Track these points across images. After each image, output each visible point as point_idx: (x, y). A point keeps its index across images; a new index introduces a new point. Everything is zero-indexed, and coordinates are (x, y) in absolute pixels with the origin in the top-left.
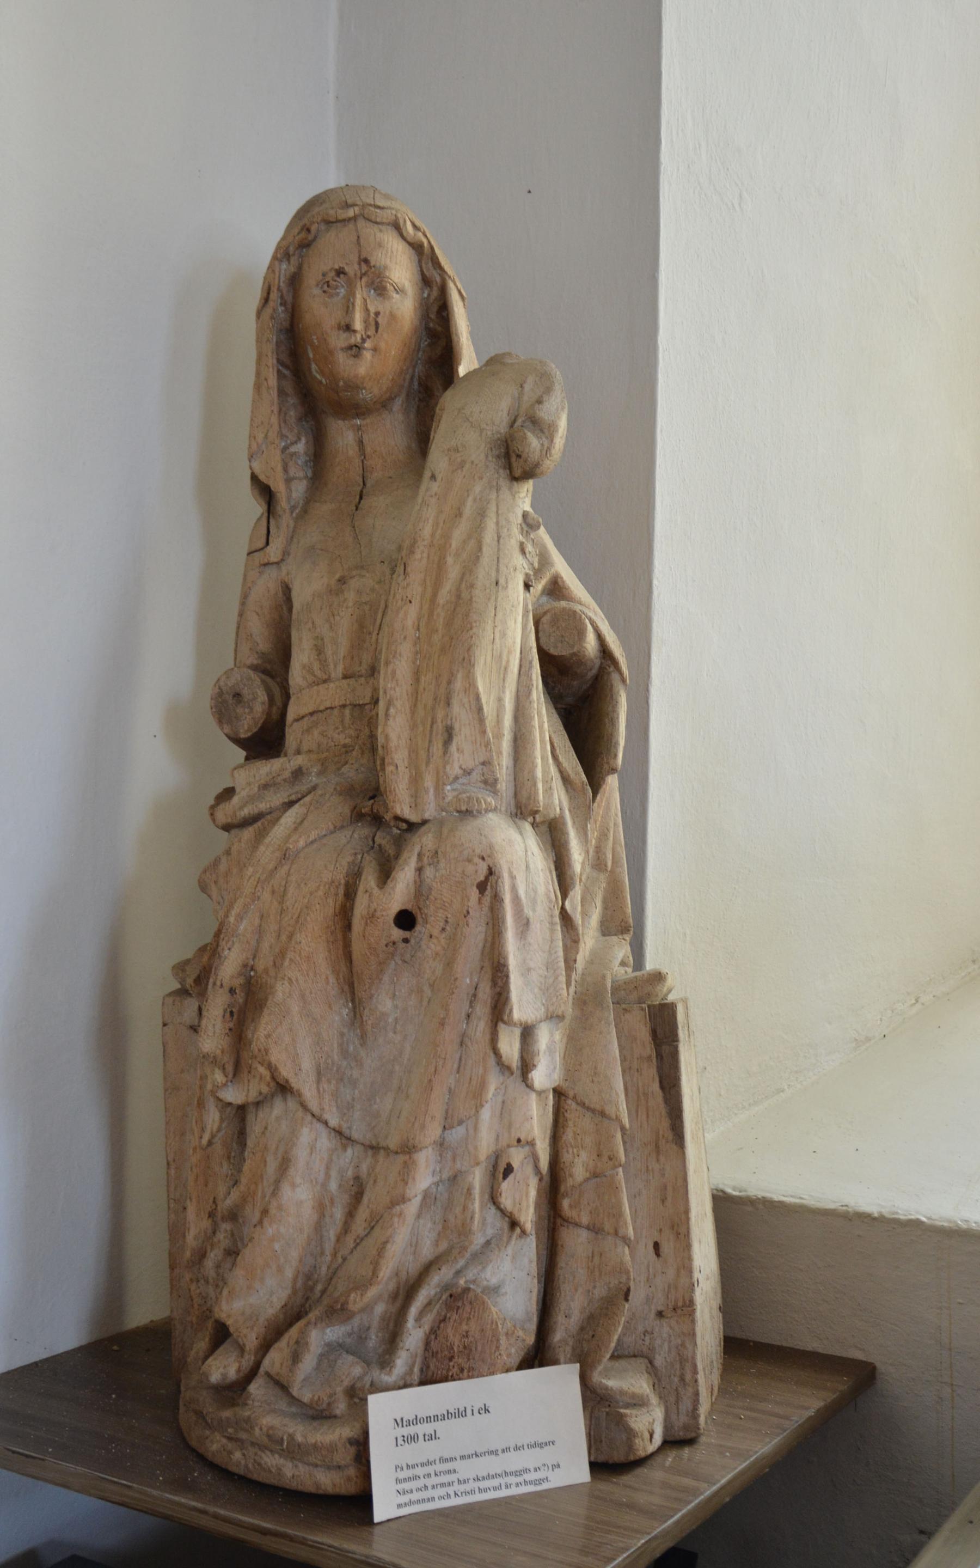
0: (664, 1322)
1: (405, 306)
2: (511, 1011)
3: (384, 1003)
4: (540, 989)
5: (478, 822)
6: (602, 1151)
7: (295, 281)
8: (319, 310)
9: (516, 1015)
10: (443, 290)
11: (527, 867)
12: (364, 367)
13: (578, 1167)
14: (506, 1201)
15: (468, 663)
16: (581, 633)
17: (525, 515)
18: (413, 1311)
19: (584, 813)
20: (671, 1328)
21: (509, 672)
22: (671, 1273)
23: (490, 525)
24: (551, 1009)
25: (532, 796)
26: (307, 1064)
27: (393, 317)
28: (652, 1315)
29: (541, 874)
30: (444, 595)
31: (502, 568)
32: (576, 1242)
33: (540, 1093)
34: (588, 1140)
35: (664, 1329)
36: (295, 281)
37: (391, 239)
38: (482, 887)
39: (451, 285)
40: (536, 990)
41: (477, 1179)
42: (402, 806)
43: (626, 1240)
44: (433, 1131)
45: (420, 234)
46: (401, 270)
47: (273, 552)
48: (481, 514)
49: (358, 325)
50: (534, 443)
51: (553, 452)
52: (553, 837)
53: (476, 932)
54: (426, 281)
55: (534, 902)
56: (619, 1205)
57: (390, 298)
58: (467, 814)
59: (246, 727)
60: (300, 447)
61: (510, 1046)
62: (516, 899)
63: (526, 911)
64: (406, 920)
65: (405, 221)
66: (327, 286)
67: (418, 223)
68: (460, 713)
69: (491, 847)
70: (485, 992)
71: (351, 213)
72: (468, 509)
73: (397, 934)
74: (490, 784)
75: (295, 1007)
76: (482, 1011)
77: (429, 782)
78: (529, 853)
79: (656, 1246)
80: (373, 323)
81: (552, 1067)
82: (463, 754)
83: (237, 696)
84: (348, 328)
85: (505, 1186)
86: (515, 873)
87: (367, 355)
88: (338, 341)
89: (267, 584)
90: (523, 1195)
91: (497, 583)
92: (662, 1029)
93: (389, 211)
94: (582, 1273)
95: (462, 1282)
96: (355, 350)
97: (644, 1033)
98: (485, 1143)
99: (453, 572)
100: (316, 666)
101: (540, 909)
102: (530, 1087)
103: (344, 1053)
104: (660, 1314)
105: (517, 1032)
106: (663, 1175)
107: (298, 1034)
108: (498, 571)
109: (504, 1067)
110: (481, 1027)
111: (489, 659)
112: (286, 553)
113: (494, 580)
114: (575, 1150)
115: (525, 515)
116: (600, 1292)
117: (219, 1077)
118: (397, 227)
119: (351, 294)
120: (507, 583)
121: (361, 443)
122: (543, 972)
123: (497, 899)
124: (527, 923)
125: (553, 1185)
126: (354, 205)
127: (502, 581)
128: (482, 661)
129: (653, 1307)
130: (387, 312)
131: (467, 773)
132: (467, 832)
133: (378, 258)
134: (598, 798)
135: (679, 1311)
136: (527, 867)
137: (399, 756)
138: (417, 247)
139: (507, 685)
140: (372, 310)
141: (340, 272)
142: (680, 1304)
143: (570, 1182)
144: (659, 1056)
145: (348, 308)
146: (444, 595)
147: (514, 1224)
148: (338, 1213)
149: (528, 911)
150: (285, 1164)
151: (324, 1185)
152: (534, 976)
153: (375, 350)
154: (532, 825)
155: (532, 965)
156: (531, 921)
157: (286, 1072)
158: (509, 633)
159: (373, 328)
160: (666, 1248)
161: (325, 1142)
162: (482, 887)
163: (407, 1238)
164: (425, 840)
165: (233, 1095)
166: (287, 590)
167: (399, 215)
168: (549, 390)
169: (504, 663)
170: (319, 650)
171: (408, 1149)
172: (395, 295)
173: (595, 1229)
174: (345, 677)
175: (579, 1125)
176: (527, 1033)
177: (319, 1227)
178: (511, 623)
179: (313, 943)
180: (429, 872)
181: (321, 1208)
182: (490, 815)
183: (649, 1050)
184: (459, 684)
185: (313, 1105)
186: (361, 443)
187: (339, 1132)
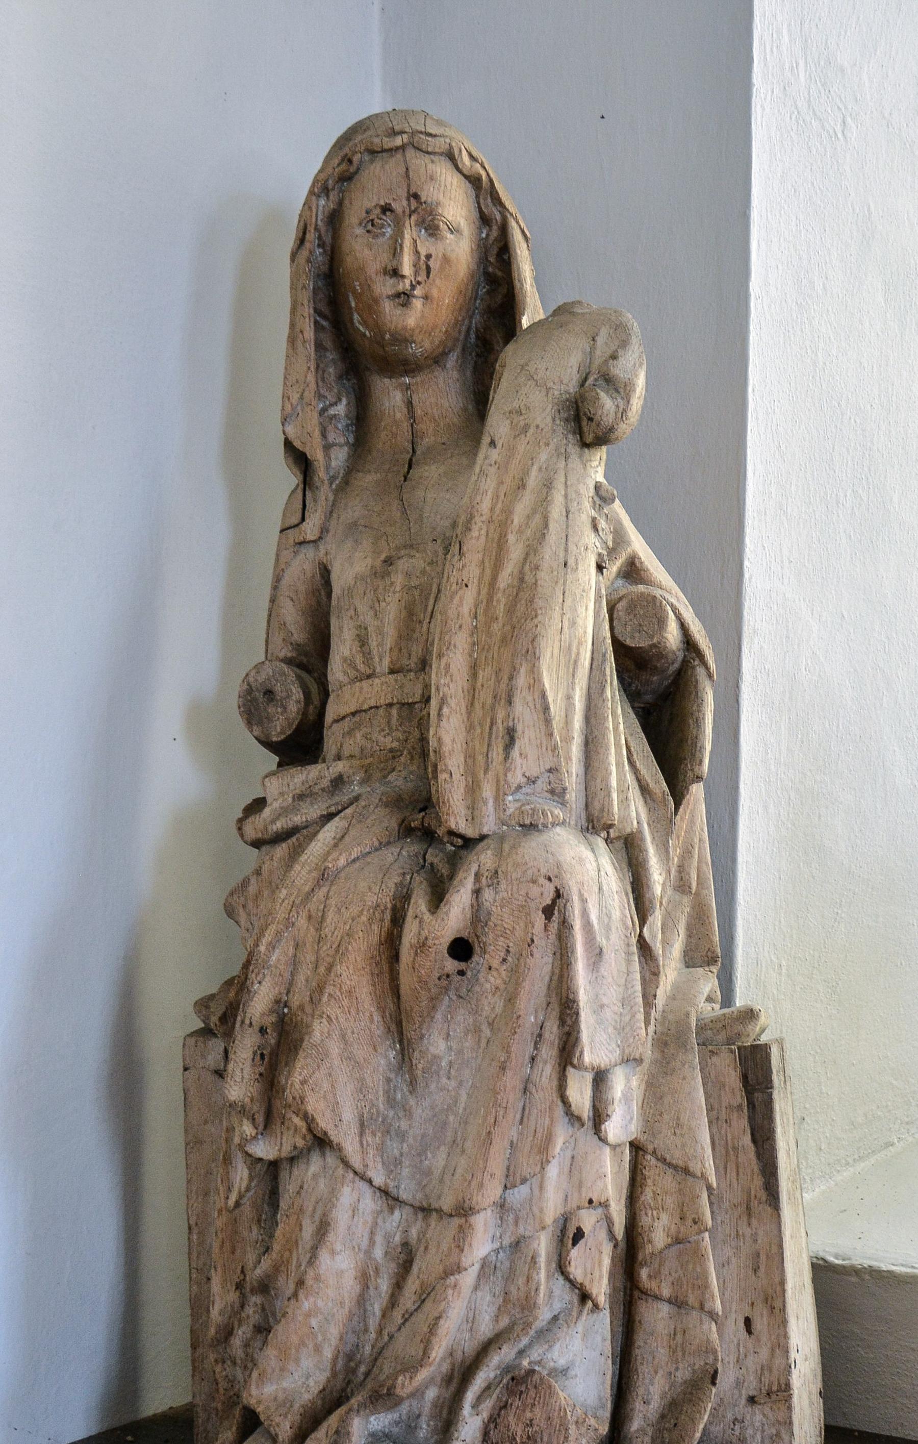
0: (757, 1409)
1: (460, 248)
2: (582, 1053)
3: (437, 1044)
4: (615, 1028)
5: (544, 837)
6: (686, 1214)
7: (335, 219)
8: (363, 252)
9: (587, 1058)
10: (504, 229)
11: (600, 889)
12: (413, 318)
13: (659, 1231)
14: (576, 1271)
15: (532, 656)
16: (661, 622)
17: (598, 487)
18: (470, 1396)
19: (665, 828)
20: (764, 1415)
21: (580, 666)
22: (765, 1353)
23: (558, 498)
24: (627, 1051)
25: (606, 808)
26: (349, 1114)
27: (446, 260)
28: (743, 1401)
29: (616, 897)
30: (505, 579)
31: (572, 547)
32: (656, 1318)
33: (614, 1147)
34: (670, 1201)
35: (757, 1417)
36: (335, 219)
37: (444, 171)
38: (548, 912)
39: (513, 224)
40: (610, 1030)
41: (543, 1245)
42: (457, 819)
43: (712, 1315)
44: (493, 1191)
45: (478, 165)
46: (455, 206)
47: (310, 529)
48: (548, 485)
49: (407, 269)
50: (607, 404)
51: (630, 414)
52: (629, 852)
53: (541, 964)
54: (484, 220)
55: (608, 928)
56: (705, 1275)
57: (442, 238)
58: (530, 828)
59: (279, 729)
60: (341, 409)
61: (580, 1093)
62: (587, 926)
63: (598, 939)
64: (461, 949)
65: (460, 151)
66: (371, 225)
67: (475, 154)
68: (523, 712)
69: (559, 865)
70: (552, 1032)
71: (398, 141)
72: (533, 480)
73: (451, 965)
74: (558, 794)
75: (334, 1048)
76: (549, 1053)
77: (488, 791)
78: (602, 873)
79: (748, 1322)
80: (425, 267)
81: (628, 1117)
82: (527, 760)
83: (269, 693)
84: (395, 273)
85: (575, 1254)
86: (586, 895)
87: (417, 304)
88: (384, 287)
89: (302, 566)
90: (595, 1264)
91: (565, 565)
92: (756, 1074)
93: (442, 139)
94: (662, 1353)
95: (525, 1363)
96: (404, 298)
97: (733, 1078)
98: (552, 1205)
99: (515, 551)
100: (359, 660)
101: (614, 937)
102: (603, 1140)
103: (391, 1102)
104: (752, 1400)
105: (589, 1077)
106: (756, 1241)
107: (339, 1078)
108: (566, 550)
109: (574, 1118)
110: (547, 1071)
111: (556, 651)
112: (324, 530)
113: (562, 561)
114: (655, 1213)
115: (598, 487)
116: (683, 1374)
117: (248, 1129)
118: (451, 157)
119: (398, 235)
120: (577, 564)
121: (409, 404)
122: (618, 1008)
123: (565, 925)
124: (601, 953)
125: (630, 1253)
126: (402, 132)
127: (571, 562)
128: (549, 654)
129: (744, 1392)
130: (440, 255)
131: (532, 781)
132: (531, 850)
133: (429, 193)
134: (681, 810)
135: (774, 1397)
136: (600, 889)
137: (453, 763)
138: (474, 181)
139: (577, 681)
140: (423, 252)
141: (386, 209)
142: (775, 1388)
143: (649, 1249)
144: (751, 1105)
145: (396, 251)
146: (505, 579)
147: (585, 1297)
148: (384, 1285)
149: (601, 940)
150: (323, 1228)
151: (368, 1253)
152: (608, 1013)
153: (426, 297)
154: (606, 840)
155: (605, 1001)
156: (604, 950)
157: (324, 1123)
158: (580, 622)
159: (423, 273)
160: (760, 1325)
161: (369, 1203)
162: (548, 912)
163: (463, 1313)
164: (485, 858)
165: (264, 1150)
166: (325, 572)
167: (454, 144)
168: (624, 344)
169: (573, 656)
170: (362, 641)
171: (464, 1211)
172: (449, 235)
173: (678, 1303)
174: (392, 672)
175: (659, 1183)
176: (600, 1078)
177: (362, 1300)
178: (581, 610)
179: (355, 975)
180: (488, 895)
181: (365, 1279)
182: (558, 829)
183: (739, 1098)
184: (522, 680)
185: (356, 1161)
186: (409, 404)
187: (384, 1192)
